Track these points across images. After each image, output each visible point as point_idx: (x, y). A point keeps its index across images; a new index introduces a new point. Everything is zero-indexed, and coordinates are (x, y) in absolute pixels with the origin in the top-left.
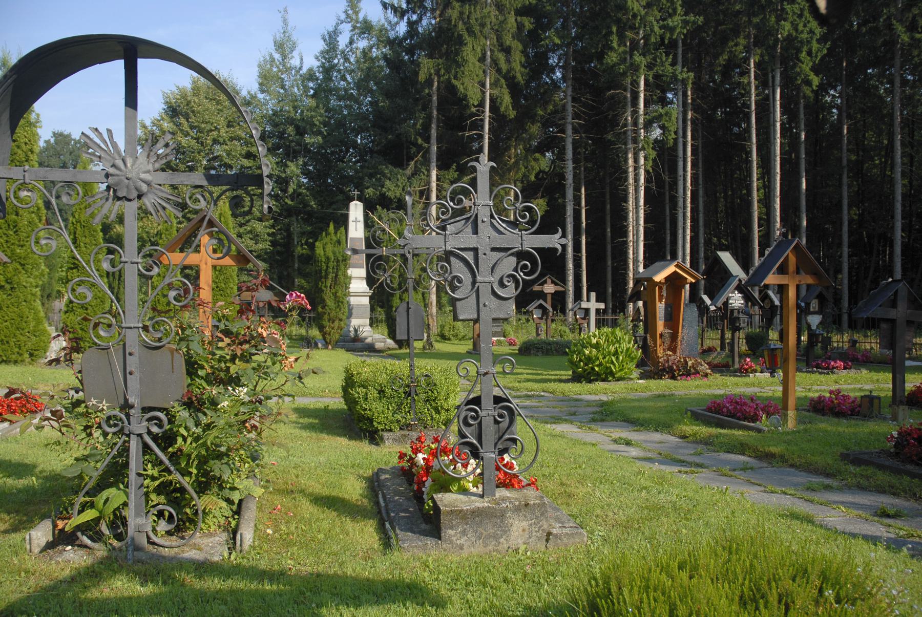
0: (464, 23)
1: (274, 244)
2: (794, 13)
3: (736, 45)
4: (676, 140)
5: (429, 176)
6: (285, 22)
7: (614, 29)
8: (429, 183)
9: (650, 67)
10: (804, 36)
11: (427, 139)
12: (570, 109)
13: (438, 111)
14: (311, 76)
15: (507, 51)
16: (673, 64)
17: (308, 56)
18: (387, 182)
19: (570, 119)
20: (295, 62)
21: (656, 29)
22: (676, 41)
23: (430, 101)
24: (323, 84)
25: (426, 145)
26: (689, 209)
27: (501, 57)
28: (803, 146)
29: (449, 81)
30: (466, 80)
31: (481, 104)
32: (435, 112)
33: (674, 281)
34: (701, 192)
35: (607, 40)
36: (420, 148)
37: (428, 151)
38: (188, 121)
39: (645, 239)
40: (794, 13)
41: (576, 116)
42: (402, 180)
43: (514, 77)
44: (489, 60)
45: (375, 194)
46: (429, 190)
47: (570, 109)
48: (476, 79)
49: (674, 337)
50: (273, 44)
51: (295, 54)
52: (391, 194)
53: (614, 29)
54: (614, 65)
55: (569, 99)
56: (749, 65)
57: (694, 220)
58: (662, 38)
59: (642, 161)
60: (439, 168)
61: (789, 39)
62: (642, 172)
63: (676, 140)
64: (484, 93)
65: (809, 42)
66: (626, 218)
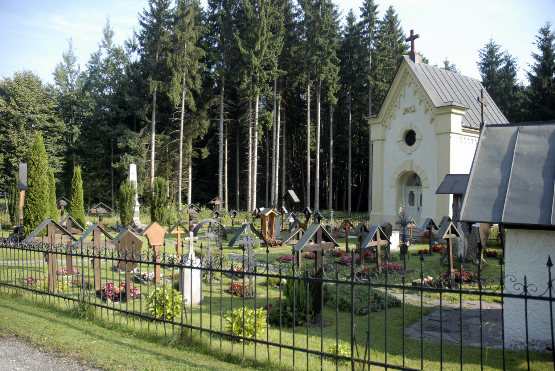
0: (173, 63)
1: (63, 168)
2: (326, 71)
3: (302, 77)
4: (272, 127)
5: (151, 137)
6: (71, 46)
7: (246, 72)
8: (151, 141)
9: (262, 91)
10: (331, 81)
11: (150, 118)
12: (223, 106)
13: (156, 104)
14: (84, 74)
15: (193, 78)
16: (273, 90)
17: (82, 65)
18: (130, 140)
19: (222, 111)
20: (75, 68)
21: (265, 75)
22: (274, 81)
23: (152, 97)
24: (90, 82)
25: (149, 121)
26: (278, 155)
27: (190, 81)
28: (332, 125)
29: (165, 93)
30: (174, 94)
31: (180, 105)
32: (155, 105)
33: (272, 215)
34: (284, 131)
35: (242, 77)
36: (146, 123)
37: (150, 124)
38: (15, 100)
39: (257, 172)
40: (326, 71)
41: (225, 109)
42: (137, 140)
43: (196, 91)
44: (185, 83)
45: (123, 146)
46: (151, 145)
47: (223, 106)
48: (178, 93)
49: (271, 233)
50: (62, 56)
51: (76, 64)
52: (131, 147)
53: (246, 72)
54: (245, 90)
55: (222, 101)
56: (307, 88)
57: (281, 159)
58: (268, 79)
59: (256, 135)
60: (156, 133)
61: (325, 82)
62: (256, 140)
63: (272, 127)
64: (181, 99)
65: (332, 84)
66: (247, 160)
